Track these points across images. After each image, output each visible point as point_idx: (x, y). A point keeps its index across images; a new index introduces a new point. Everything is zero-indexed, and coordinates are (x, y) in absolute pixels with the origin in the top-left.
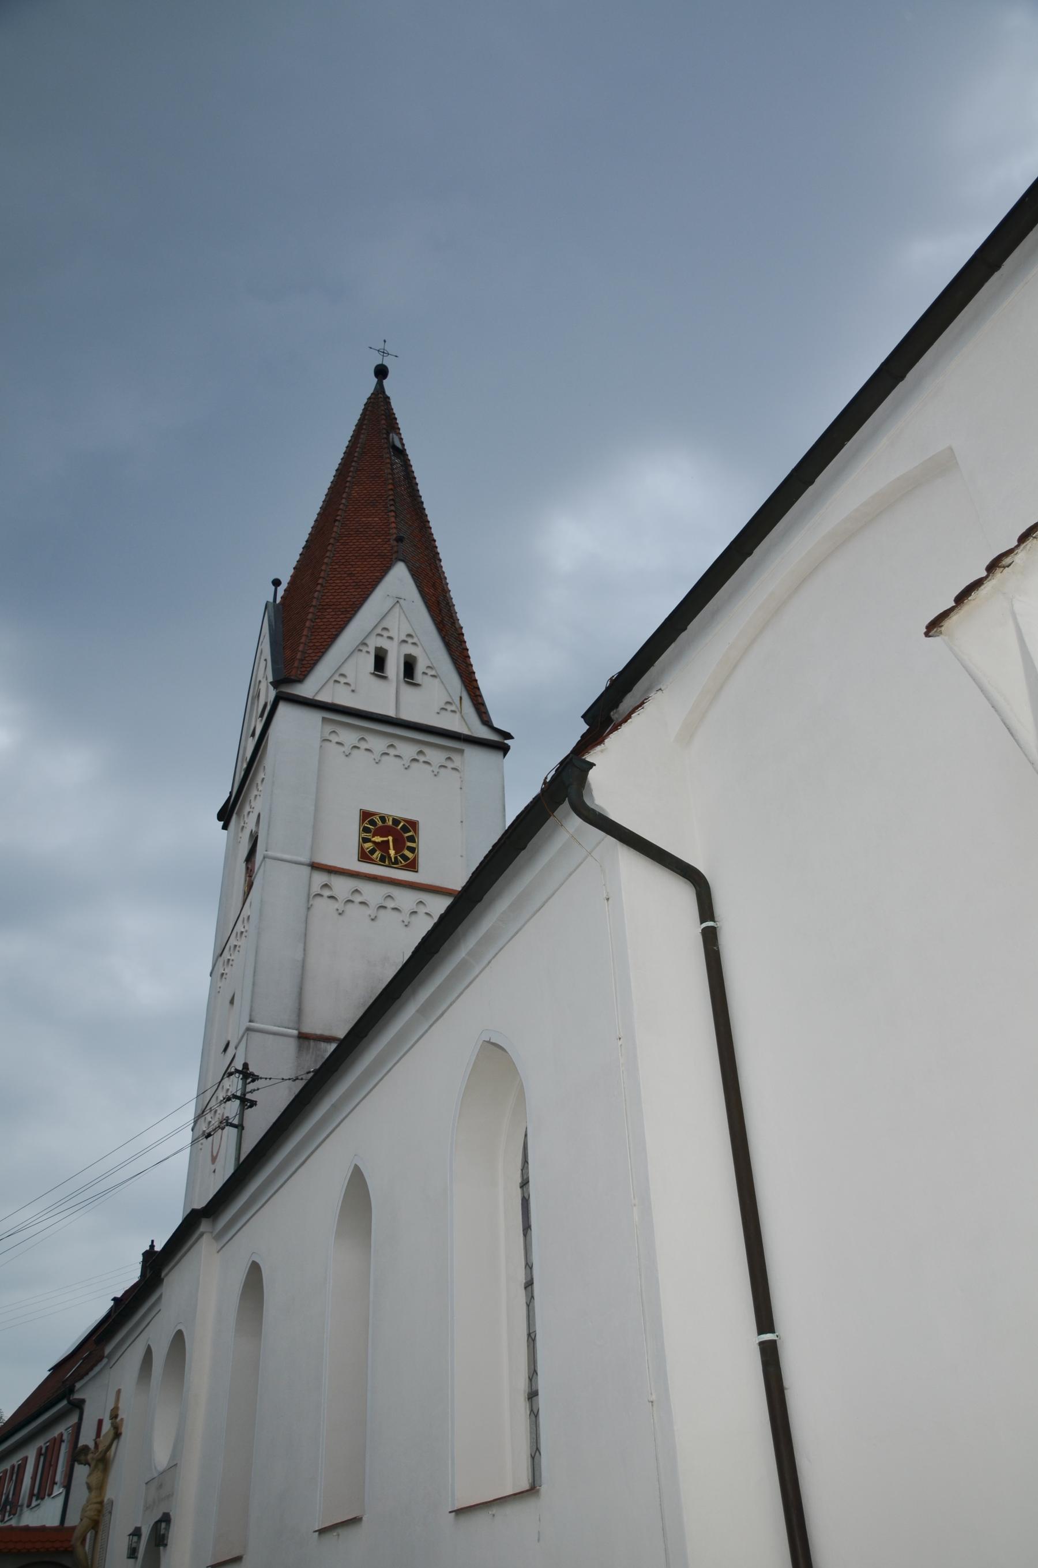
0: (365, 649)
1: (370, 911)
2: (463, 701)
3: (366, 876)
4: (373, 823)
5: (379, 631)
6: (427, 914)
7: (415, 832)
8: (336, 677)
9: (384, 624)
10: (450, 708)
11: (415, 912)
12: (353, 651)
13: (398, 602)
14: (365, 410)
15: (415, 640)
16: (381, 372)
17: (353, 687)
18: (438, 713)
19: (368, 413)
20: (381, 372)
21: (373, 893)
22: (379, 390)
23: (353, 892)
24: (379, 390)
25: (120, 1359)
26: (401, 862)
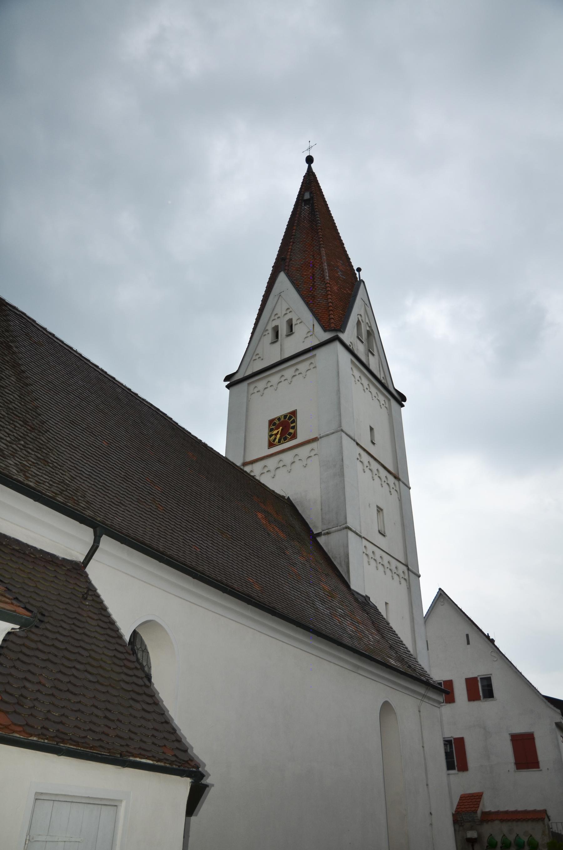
0: (266, 333)
1: (271, 474)
2: (315, 326)
3: (302, 444)
4: (290, 418)
5: (273, 318)
6: (299, 460)
7: (295, 417)
8: (254, 358)
9: (275, 313)
10: (309, 334)
11: (294, 462)
12: (261, 336)
13: (280, 295)
14: (302, 186)
15: (291, 310)
16: (310, 160)
17: (262, 358)
18: (303, 342)
19: (303, 187)
20: (310, 160)
21: (287, 457)
22: (310, 170)
23: (279, 462)
24: (310, 170)
25: (361, 676)
26: (288, 438)
